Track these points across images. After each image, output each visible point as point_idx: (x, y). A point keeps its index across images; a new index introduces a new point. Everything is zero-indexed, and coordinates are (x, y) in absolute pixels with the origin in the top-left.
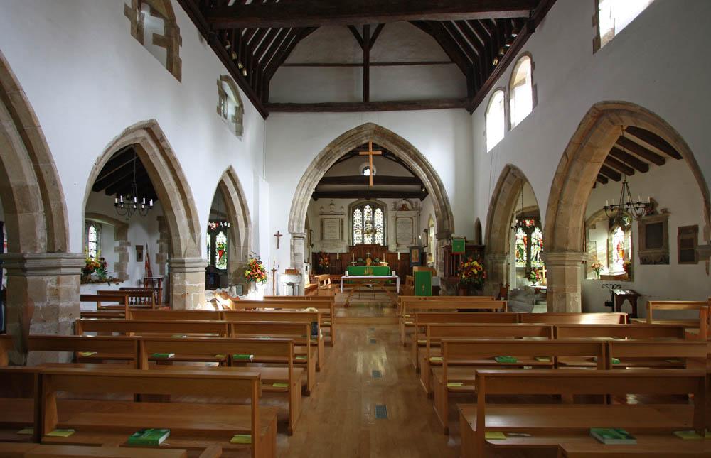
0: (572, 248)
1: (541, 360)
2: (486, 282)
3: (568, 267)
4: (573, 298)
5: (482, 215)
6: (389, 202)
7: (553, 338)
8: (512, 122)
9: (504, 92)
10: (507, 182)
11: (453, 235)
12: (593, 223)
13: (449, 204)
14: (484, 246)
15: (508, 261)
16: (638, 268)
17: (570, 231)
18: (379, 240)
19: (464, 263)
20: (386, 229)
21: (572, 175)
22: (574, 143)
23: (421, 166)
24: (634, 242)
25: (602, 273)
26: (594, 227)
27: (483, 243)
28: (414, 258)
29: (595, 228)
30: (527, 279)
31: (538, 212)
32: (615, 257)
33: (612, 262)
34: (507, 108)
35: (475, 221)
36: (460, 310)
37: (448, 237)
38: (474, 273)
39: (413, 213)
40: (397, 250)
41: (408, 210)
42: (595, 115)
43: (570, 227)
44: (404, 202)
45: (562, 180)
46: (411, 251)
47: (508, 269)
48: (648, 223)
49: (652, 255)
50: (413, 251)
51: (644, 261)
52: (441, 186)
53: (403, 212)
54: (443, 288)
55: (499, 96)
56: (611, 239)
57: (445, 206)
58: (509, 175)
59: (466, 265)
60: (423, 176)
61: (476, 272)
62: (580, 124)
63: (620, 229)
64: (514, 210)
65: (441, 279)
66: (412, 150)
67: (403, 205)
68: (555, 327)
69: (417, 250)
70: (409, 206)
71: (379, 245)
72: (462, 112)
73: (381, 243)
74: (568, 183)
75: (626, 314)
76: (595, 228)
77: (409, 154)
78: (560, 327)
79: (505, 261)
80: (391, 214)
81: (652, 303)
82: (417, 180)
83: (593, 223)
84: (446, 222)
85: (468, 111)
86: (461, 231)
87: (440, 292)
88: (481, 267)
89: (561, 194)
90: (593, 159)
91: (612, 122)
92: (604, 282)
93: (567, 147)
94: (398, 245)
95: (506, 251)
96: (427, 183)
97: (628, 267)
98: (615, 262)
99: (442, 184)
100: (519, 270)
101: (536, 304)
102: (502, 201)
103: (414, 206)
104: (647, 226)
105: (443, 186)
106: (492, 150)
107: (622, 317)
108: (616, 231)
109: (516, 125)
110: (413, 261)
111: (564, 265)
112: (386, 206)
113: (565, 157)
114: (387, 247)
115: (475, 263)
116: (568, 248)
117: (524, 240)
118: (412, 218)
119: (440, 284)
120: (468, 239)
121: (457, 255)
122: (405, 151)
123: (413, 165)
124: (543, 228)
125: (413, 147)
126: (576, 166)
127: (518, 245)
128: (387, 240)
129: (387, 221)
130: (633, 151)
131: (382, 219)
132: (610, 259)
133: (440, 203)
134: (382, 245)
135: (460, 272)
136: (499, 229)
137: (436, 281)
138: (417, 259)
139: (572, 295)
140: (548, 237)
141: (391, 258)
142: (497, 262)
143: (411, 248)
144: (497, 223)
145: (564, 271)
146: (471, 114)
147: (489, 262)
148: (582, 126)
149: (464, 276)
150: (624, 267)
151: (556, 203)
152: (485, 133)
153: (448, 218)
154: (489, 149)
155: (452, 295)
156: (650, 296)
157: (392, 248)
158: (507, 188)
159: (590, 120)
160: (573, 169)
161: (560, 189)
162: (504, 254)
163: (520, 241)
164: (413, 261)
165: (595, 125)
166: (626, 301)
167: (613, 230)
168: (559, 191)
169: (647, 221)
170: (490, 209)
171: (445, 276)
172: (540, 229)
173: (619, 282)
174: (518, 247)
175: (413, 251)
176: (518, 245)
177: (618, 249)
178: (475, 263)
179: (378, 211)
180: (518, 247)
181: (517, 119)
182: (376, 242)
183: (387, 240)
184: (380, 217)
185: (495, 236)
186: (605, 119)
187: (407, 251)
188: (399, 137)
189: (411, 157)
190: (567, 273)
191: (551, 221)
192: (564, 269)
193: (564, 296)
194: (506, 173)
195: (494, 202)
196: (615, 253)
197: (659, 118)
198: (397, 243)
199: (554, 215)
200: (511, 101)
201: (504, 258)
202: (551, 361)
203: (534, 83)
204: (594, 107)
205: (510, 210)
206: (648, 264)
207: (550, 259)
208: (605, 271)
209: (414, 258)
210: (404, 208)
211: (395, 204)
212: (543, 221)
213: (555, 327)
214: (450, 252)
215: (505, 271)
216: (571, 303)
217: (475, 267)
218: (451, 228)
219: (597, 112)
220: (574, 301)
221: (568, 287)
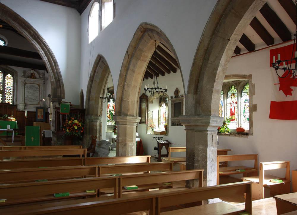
0: (131, 114)
1: (88, 192)
2: (85, 135)
3: (128, 126)
4: (131, 145)
5: (84, 87)
6: (20, 70)
7: (97, 175)
8: (103, 26)
9: (99, 4)
10: (99, 66)
11: (63, 100)
12: (151, 100)
13: (61, 76)
14: (85, 110)
15: (100, 120)
16: (171, 128)
17: (130, 103)
18: (9, 99)
19: (69, 121)
20: (15, 91)
21: (131, 67)
22: (131, 46)
23: (40, 44)
24: (169, 113)
25: (155, 130)
26: (152, 102)
27: (84, 107)
28: (40, 116)
29: (152, 103)
30: (113, 133)
31: (113, 90)
32: (161, 121)
33: (160, 124)
34: (100, 15)
35: (80, 92)
36: (64, 156)
37: (60, 102)
38: (75, 128)
39: (41, 81)
40: (24, 109)
41: (36, 78)
42: (142, 30)
43: (130, 100)
44: (32, 71)
45: (126, 69)
46: (37, 110)
47: (100, 126)
48: (175, 102)
49: (176, 121)
50: (39, 110)
51: (173, 124)
52: (55, 62)
53: (32, 80)
54: (55, 139)
55: (96, 6)
56: (160, 110)
57: (59, 79)
58: (101, 62)
59: (70, 122)
60: (42, 53)
61: (76, 127)
62: (134, 35)
63: (164, 104)
64: (105, 86)
65: (53, 132)
66: (33, 31)
67: (32, 74)
68: (99, 168)
69: (42, 110)
70: (37, 75)
71: (8, 104)
72: (73, 12)
73: (11, 102)
74: (129, 71)
75: (150, 156)
76: (152, 103)
77: (30, 33)
78: (102, 168)
79: (99, 121)
80: (21, 80)
81: (171, 148)
82: (37, 56)
83: (151, 100)
84: (59, 90)
85: (78, 12)
86: (69, 97)
87: (52, 142)
88: (80, 124)
89: (125, 78)
90: (142, 58)
91: (150, 37)
92: (155, 136)
93: (128, 49)
94: (26, 105)
95: (99, 114)
96: (45, 59)
97: (166, 127)
98: (161, 124)
99: (56, 61)
100: (109, 127)
101: (112, 150)
102: (97, 79)
103: (41, 76)
104: (175, 104)
105: (57, 63)
106: (91, 43)
107: (148, 158)
108: (162, 105)
109: (105, 28)
110: (38, 118)
111: (126, 125)
112: (16, 72)
113: (127, 54)
114: (16, 106)
115: (76, 121)
116: (129, 114)
117: (113, 107)
118: (39, 85)
119: (51, 136)
120: (72, 103)
121: (64, 115)
122: (26, 30)
123: (32, 42)
124: (115, 100)
125: (33, 28)
126: (133, 61)
127: (110, 110)
128: (16, 101)
129: (17, 85)
130: (165, 56)
131: (12, 83)
132: (159, 122)
133: (55, 75)
134: (11, 103)
135: (65, 128)
136: (95, 98)
137: (48, 134)
138: (41, 116)
139: (130, 144)
140: (118, 106)
141: (19, 115)
142: (93, 121)
143: (37, 108)
144: (93, 94)
145: (125, 128)
146: (81, 14)
147: (88, 121)
148: (135, 36)
149: (68, 130)
150: (165, 127)
151: (123, 84)
152: (88, 31)
153: (60, 88)
154: (90, 42)
155: (61, 145)
156: (175, 144)
157: (21, 107)
158: (99, 70)
159: (139, 33)
160: (132, 63)
161: (125, 75)
162: (97, 115)
163: (111, 108)
164: (38, 118)
165: (142, 37)
166: (164, 147)
167: (161, 105)
168: (124, 77)
169: (175, 101)
170: (89, 84)
171: (55, 130)
172: (114, 100)
173: (162, 136)
174: (110, 112)
175: (39, 110)
176: (110, 110)
177: (163, 116)
178: (76, 121)
179: (9, 76)
180: (110, 112)
181: (105, 24)
182: (6, 101)
183: (16, 101)
184: (11, 81)
185: (92, 102)
186: (146, 34)
187: (33, 110)
188: (20, 17)
189: (32, 36)
190: (128, 129)
191: (120, 95)
192: (126, 127)
193: (125, 145)
194: (98, 60)
195: (92, 79)
196: (162, 118)
197: (167, 39)
198: (25, 103)
199: (122, 92)
200: (102, 10)
201: (98, 119)
202: (95, 192)
203: (114, 3)
204: (141, 25)
205: (101, 87)
206: (175, 126)
207: (118, 120)
208: (156, 130)
209: (40, 116)
210: (32, 76)
211: (25, 72)
212: (115, 95)
213: (99, 168)
214: (59, 113)
215: (98, 127)
216: (129, 149)
217: (76, 124)
218: (62, 94)
219: (143, 29)
220: (131, 147)
221: (128, 139)
